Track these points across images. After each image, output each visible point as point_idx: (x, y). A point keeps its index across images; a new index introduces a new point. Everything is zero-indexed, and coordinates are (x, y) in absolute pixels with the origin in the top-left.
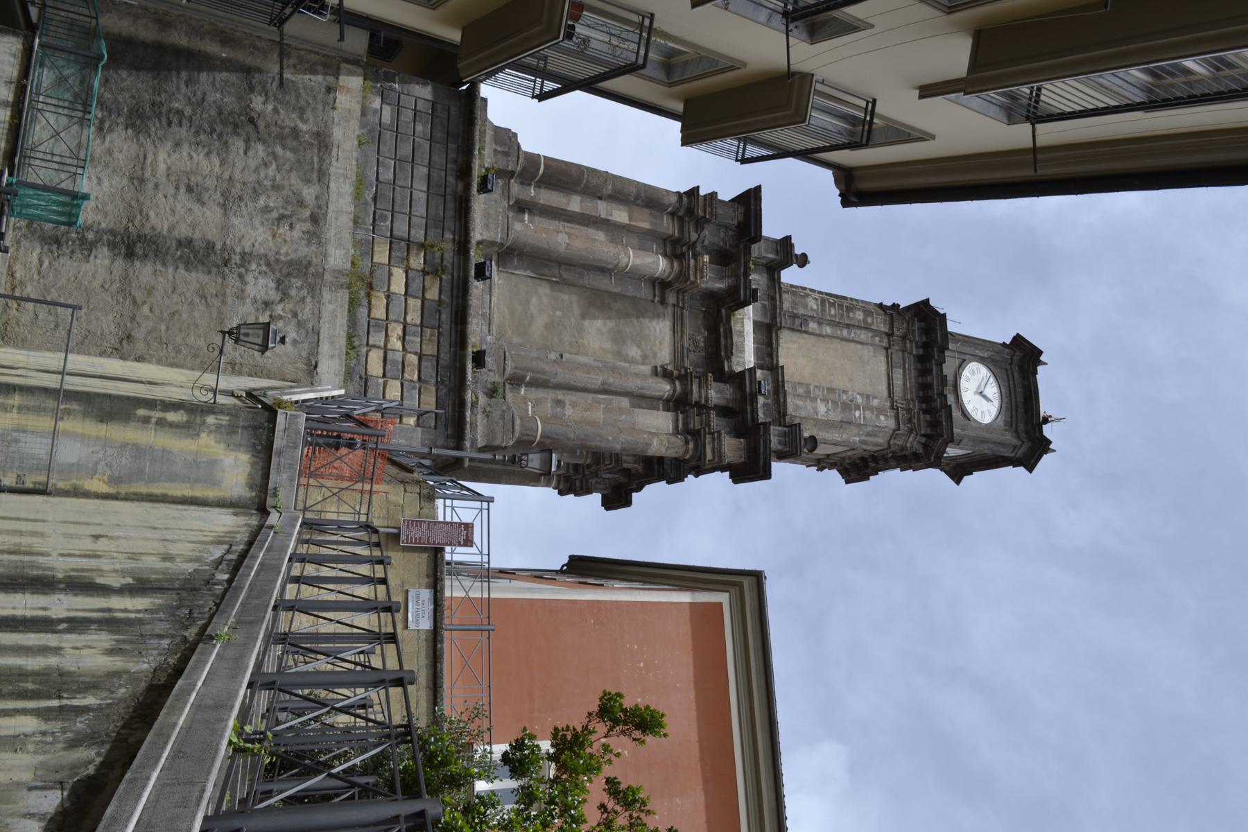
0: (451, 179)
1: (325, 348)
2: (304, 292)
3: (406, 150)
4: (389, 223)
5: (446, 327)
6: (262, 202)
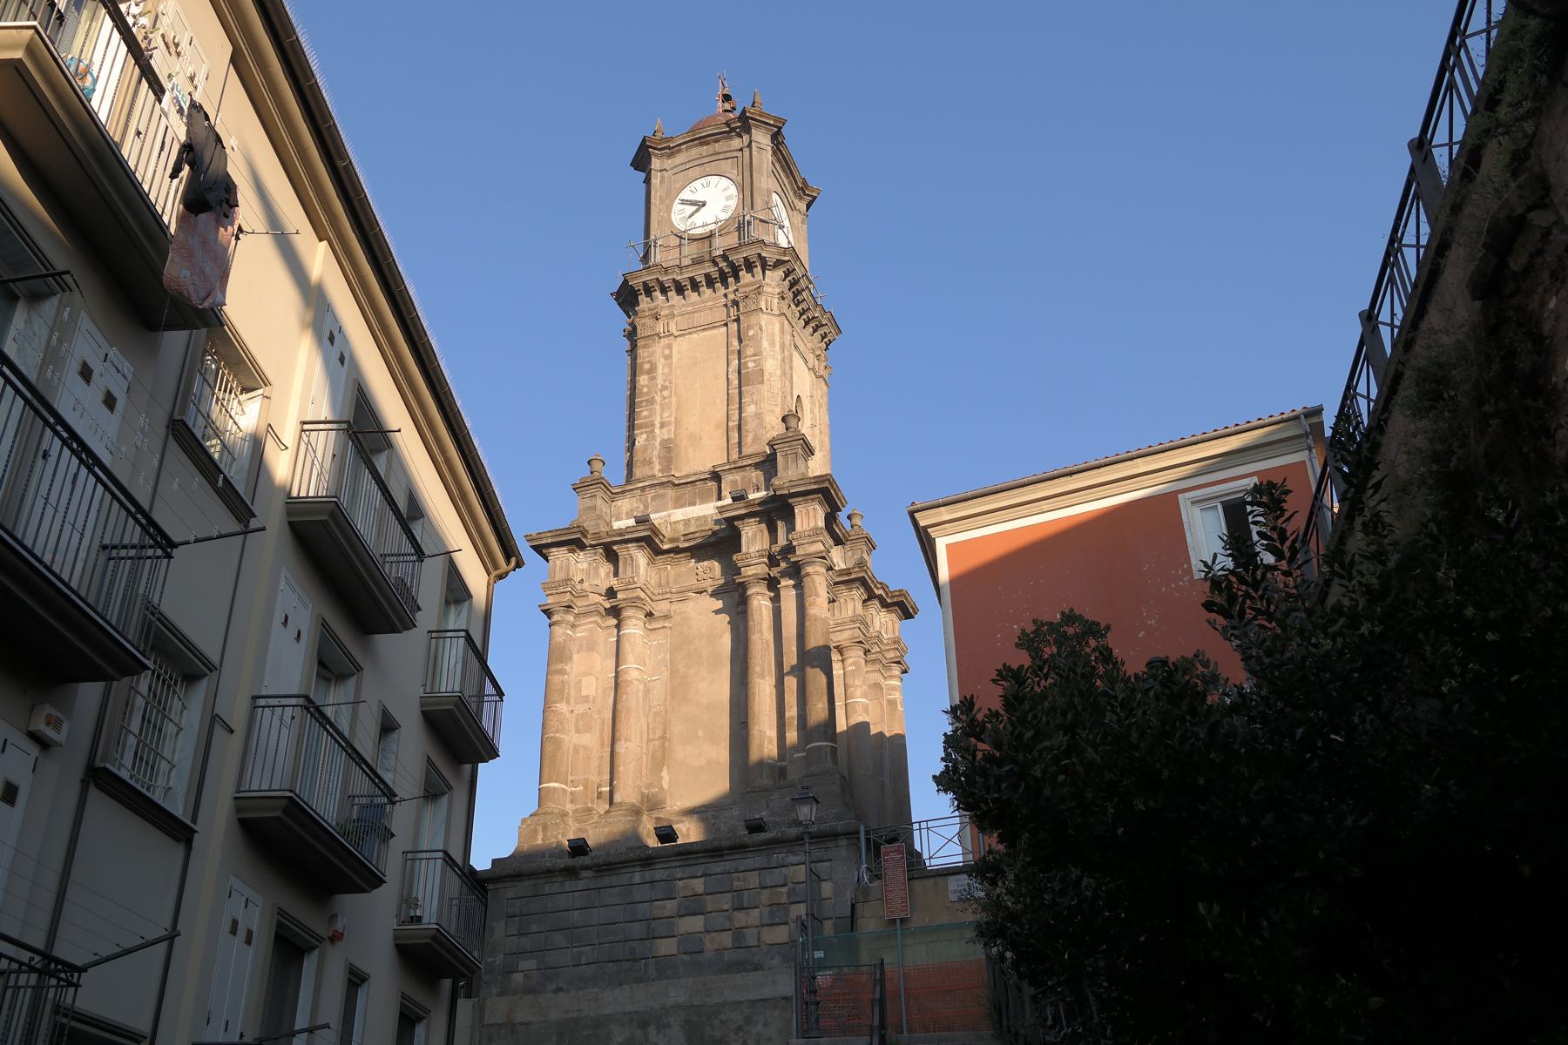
0: (581, 884)
1: (767, 992)
2: (716, 1022)
3: (559, 939)
4: (635, 944)
5: (728, 866)
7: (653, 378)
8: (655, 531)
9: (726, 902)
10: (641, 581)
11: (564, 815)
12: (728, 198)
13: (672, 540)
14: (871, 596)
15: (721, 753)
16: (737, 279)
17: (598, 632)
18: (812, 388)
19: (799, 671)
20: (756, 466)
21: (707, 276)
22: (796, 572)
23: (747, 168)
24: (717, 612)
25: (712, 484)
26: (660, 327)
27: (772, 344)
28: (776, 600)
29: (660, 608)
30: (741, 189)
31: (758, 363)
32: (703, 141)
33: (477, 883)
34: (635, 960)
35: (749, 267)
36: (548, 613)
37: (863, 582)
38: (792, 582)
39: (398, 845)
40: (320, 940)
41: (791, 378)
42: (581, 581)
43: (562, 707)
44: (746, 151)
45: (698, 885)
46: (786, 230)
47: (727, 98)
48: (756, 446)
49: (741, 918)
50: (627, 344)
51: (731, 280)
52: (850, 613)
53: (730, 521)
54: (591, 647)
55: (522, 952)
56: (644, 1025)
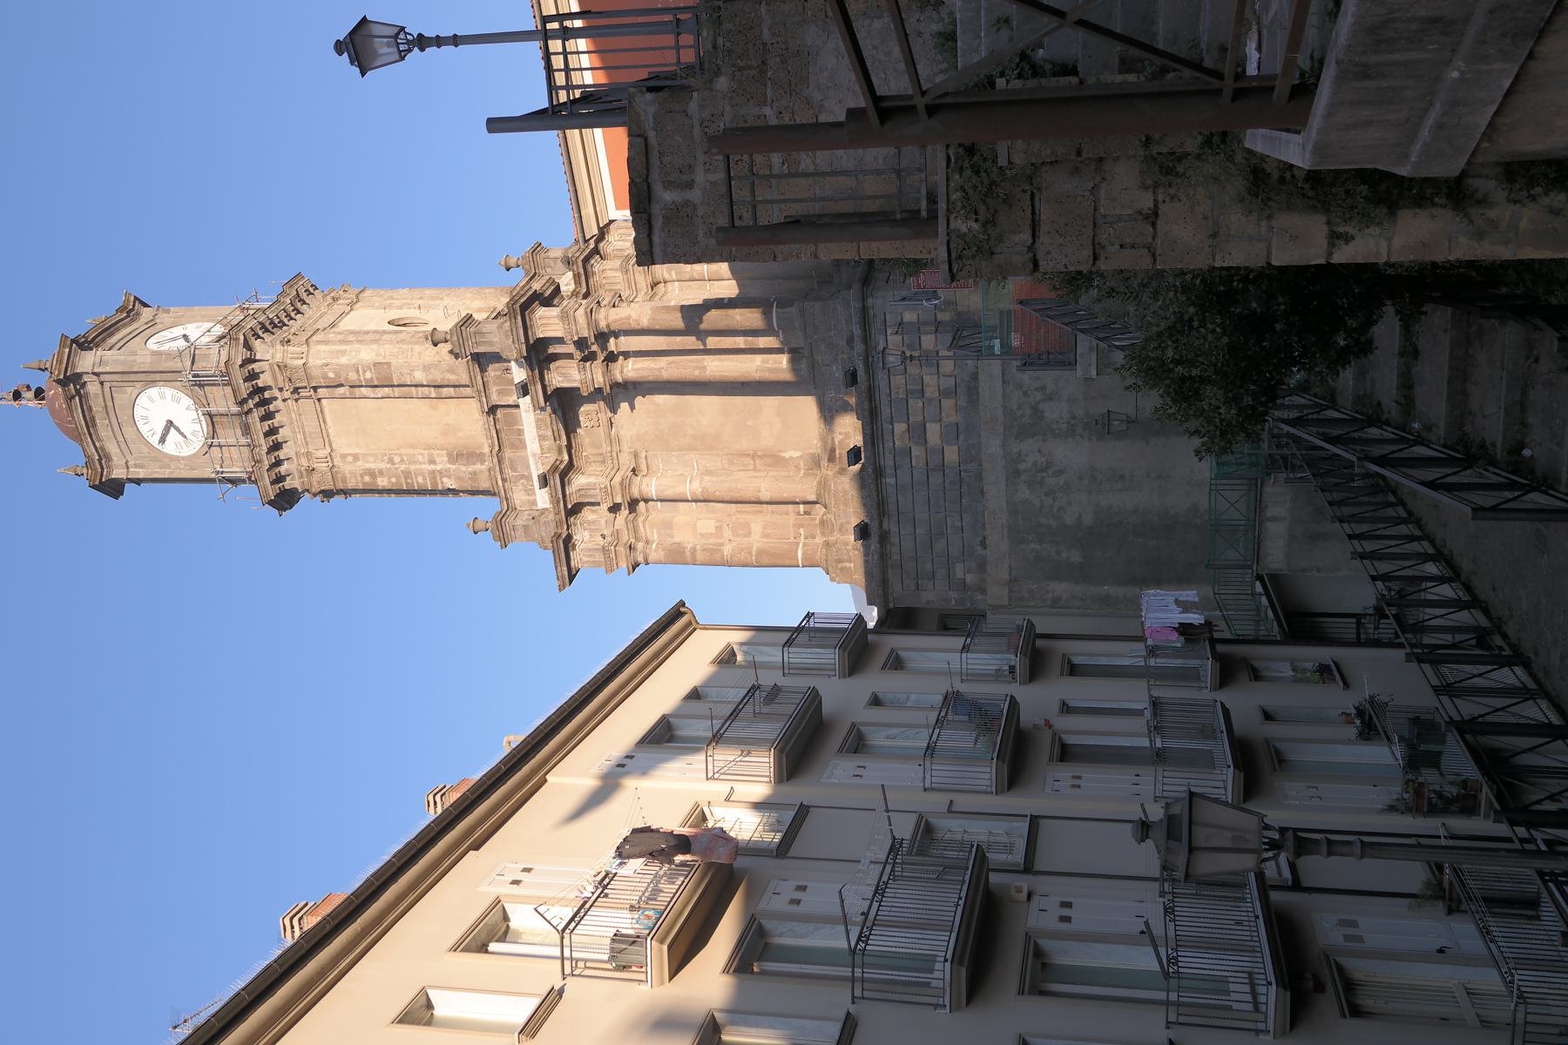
0: (894, 529)
3: (939, 545)
5: (884, 402)
6: (1062, 480)
7: (381, 473)
8: (554, 469)
9: (916, 404)
10: (604, 481)
11: (827, 545)
12: (163, 396)
13: (560, 452)
14: (596, 251)
15: (770, 404)
16: (269, 388)
17: (651, 521)
18: (373, 306)
19: (702, 335)
20: (483, 370)
21: (263, 419)
22: (602, 337)
23: (126, 377)
24: (632, 407)
25: (500, 413)
26: (322, 467)
27: (343, 353)
28: (626, 355)
29: (626, 461)
30: (153, 383)
31: (366, 368)
32: (90, 424)
33: (898, 618)
34: (961, 480)
35: (253, 376)
36: (635, 566)
37: (586, 260)
38: (612, 340)
39: (782, 681)
40: (1054, 734)
41: (362, 329)
42: (603, 536)
43: (727, 550)
44: (102, 378)
45: (900, 428)
46: (194, 331)
47: (17, 396)
48: (461, 371)
49: (931, 392)
50: (338, 499)
51: (267, 395)
52: (619, 274)
53: (547, 398)
54: (668, 525)
55: (949, 576)
56: (1017, 473)
